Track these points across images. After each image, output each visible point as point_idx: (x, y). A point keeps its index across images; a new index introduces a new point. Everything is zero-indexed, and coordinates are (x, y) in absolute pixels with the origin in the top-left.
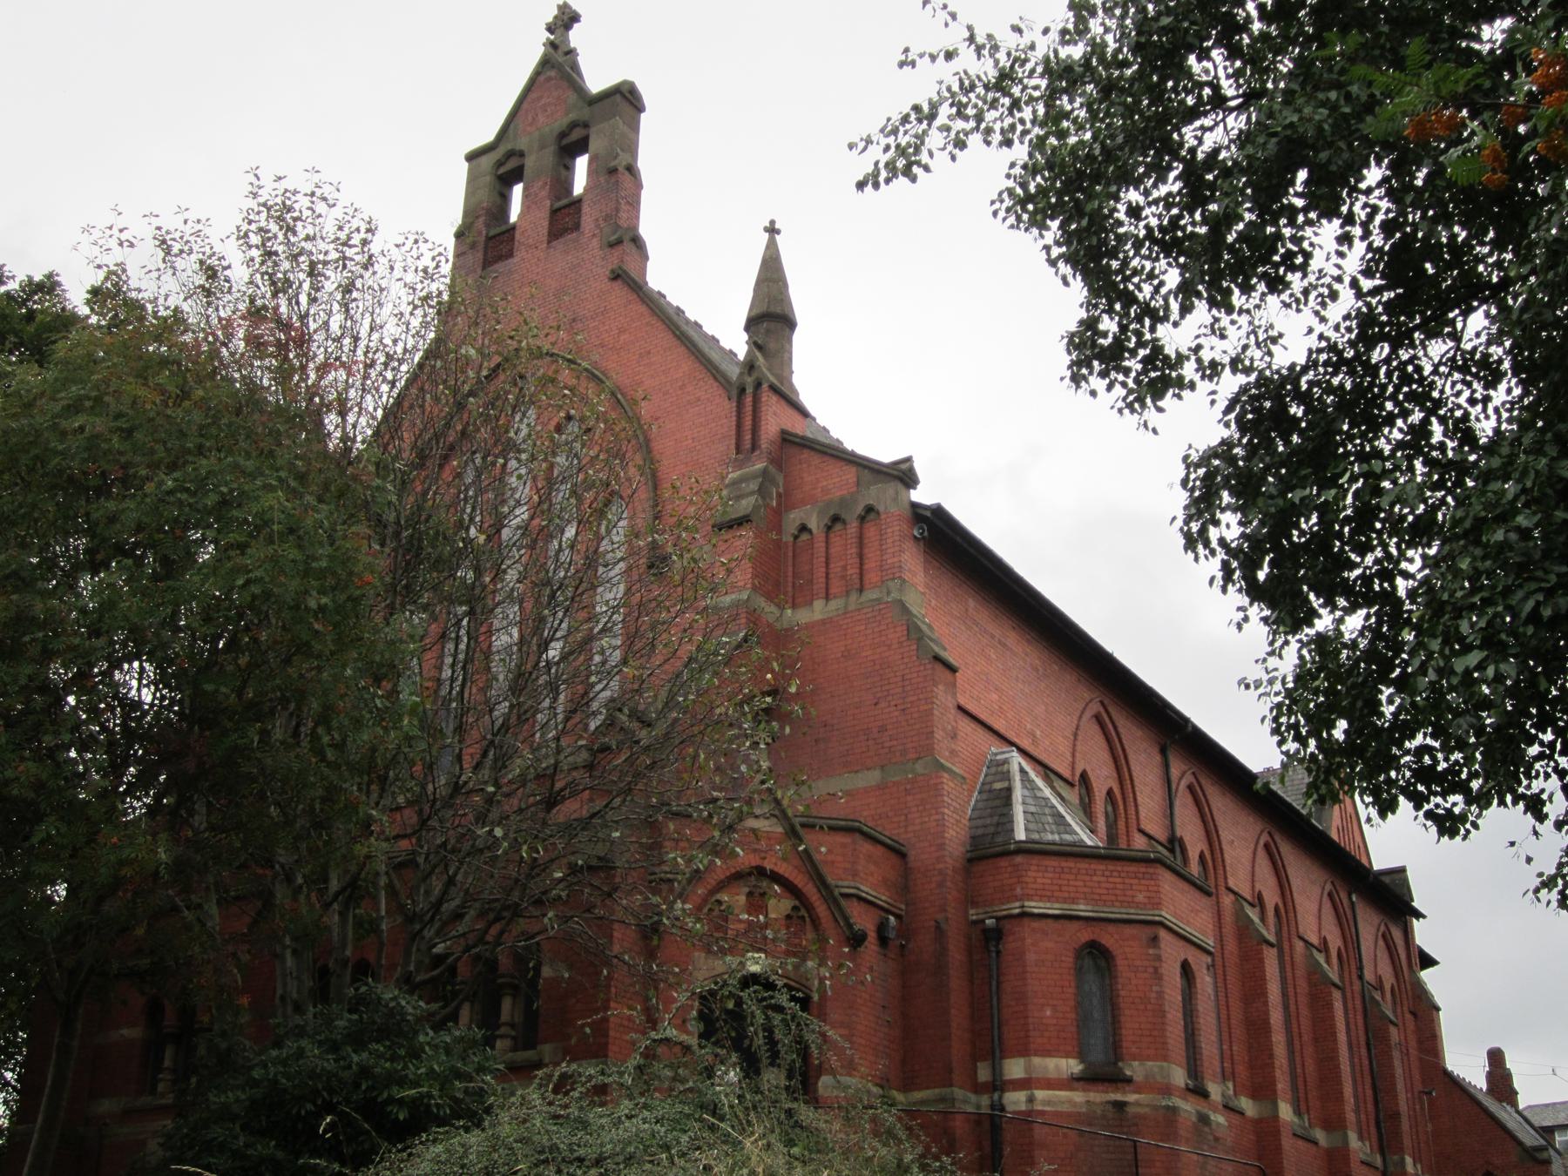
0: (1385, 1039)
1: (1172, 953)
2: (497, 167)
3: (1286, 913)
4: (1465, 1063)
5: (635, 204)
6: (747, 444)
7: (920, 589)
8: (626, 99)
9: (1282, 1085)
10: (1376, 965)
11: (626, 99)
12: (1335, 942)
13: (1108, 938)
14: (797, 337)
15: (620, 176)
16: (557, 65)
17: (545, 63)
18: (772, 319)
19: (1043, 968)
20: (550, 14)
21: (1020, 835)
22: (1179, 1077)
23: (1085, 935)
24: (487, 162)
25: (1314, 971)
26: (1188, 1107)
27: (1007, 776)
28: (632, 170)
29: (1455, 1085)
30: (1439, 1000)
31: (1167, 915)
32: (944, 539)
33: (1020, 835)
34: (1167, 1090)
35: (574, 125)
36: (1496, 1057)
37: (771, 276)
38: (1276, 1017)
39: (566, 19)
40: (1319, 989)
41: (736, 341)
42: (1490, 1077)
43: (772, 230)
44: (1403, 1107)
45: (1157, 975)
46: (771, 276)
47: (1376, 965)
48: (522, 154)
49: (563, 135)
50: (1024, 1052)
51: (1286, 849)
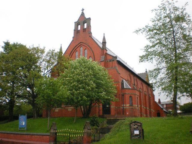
0: (150, 99)
1: (136, 96)
2: (77, 24)
3: (143, 89)
4: (157, 100)
5: (90, 29)
6: (103, 54)
7: (118, 68)
8: (90, 19)
9: (142, 104)
10: (150, 92)
11: (90, 19)
12: (146, 91)
13: (132, 95)
14: (106, 44)
15: (89, 26)
16: (83, 14)
17: (82, 14)
18: (104, 43)
19: (127, 97)
20: (82, 9)
21: (125, 88)
22: (137, 106)
23: (130, 95)
24: (77, 23)
25: (145, 94)
26: (137, 108)
27: (123, 81)
28: (90, 26)
29: (155, 102)
30: (155, 95)
31: (136, 94)
32: (120, 63)
33: (125, 88)
34: (136, 107)
35: (85, 21)
36: (159, 99)
37: (104, 39)
38: (142, 98)
39: (83, 10)
40: (145, 95)
41: (101, 46)
42: (159, 101)
43: (104, 34)
44: (152, 105)
45: (135, 98)
46: (104, 39)
47: (150, 92)
48: (80, 23)
49: (84, 22)
50: (126, 104)
51: (143, 83)
